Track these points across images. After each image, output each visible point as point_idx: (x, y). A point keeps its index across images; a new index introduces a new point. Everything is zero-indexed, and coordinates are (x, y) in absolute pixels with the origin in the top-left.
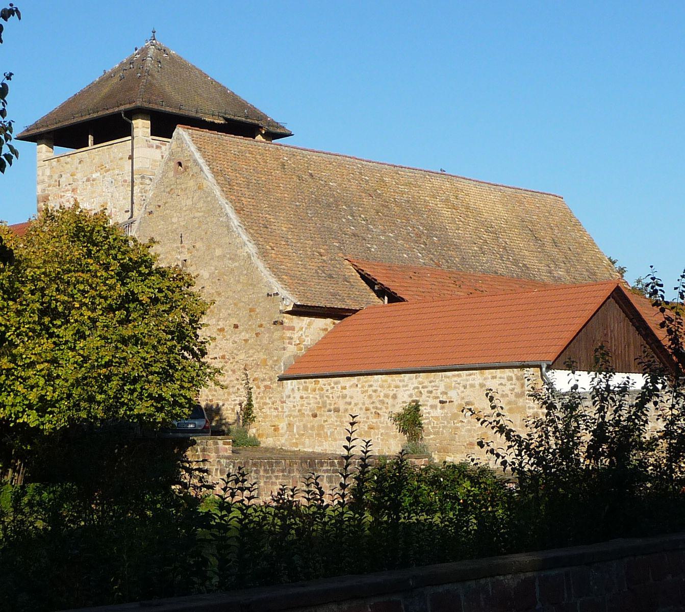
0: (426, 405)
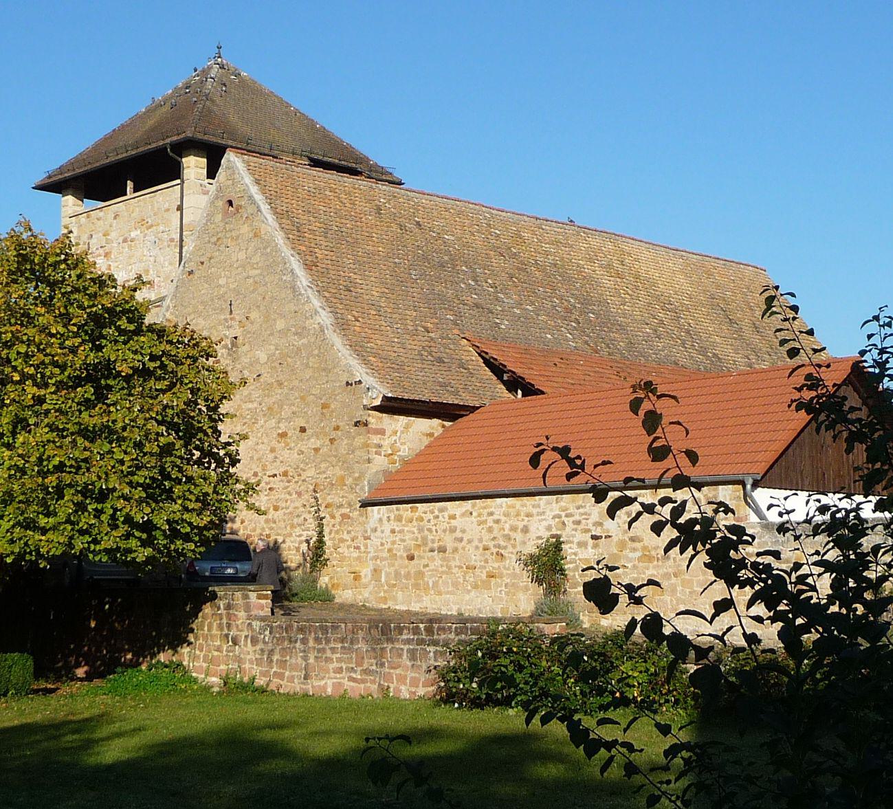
0: (572, 542)
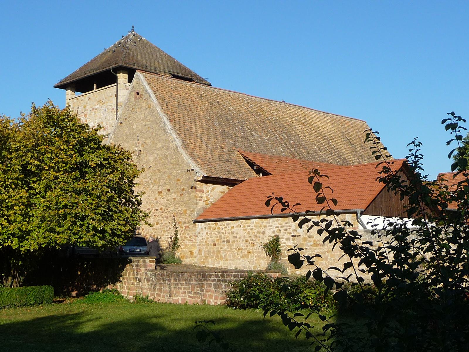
0: (283, 238)
